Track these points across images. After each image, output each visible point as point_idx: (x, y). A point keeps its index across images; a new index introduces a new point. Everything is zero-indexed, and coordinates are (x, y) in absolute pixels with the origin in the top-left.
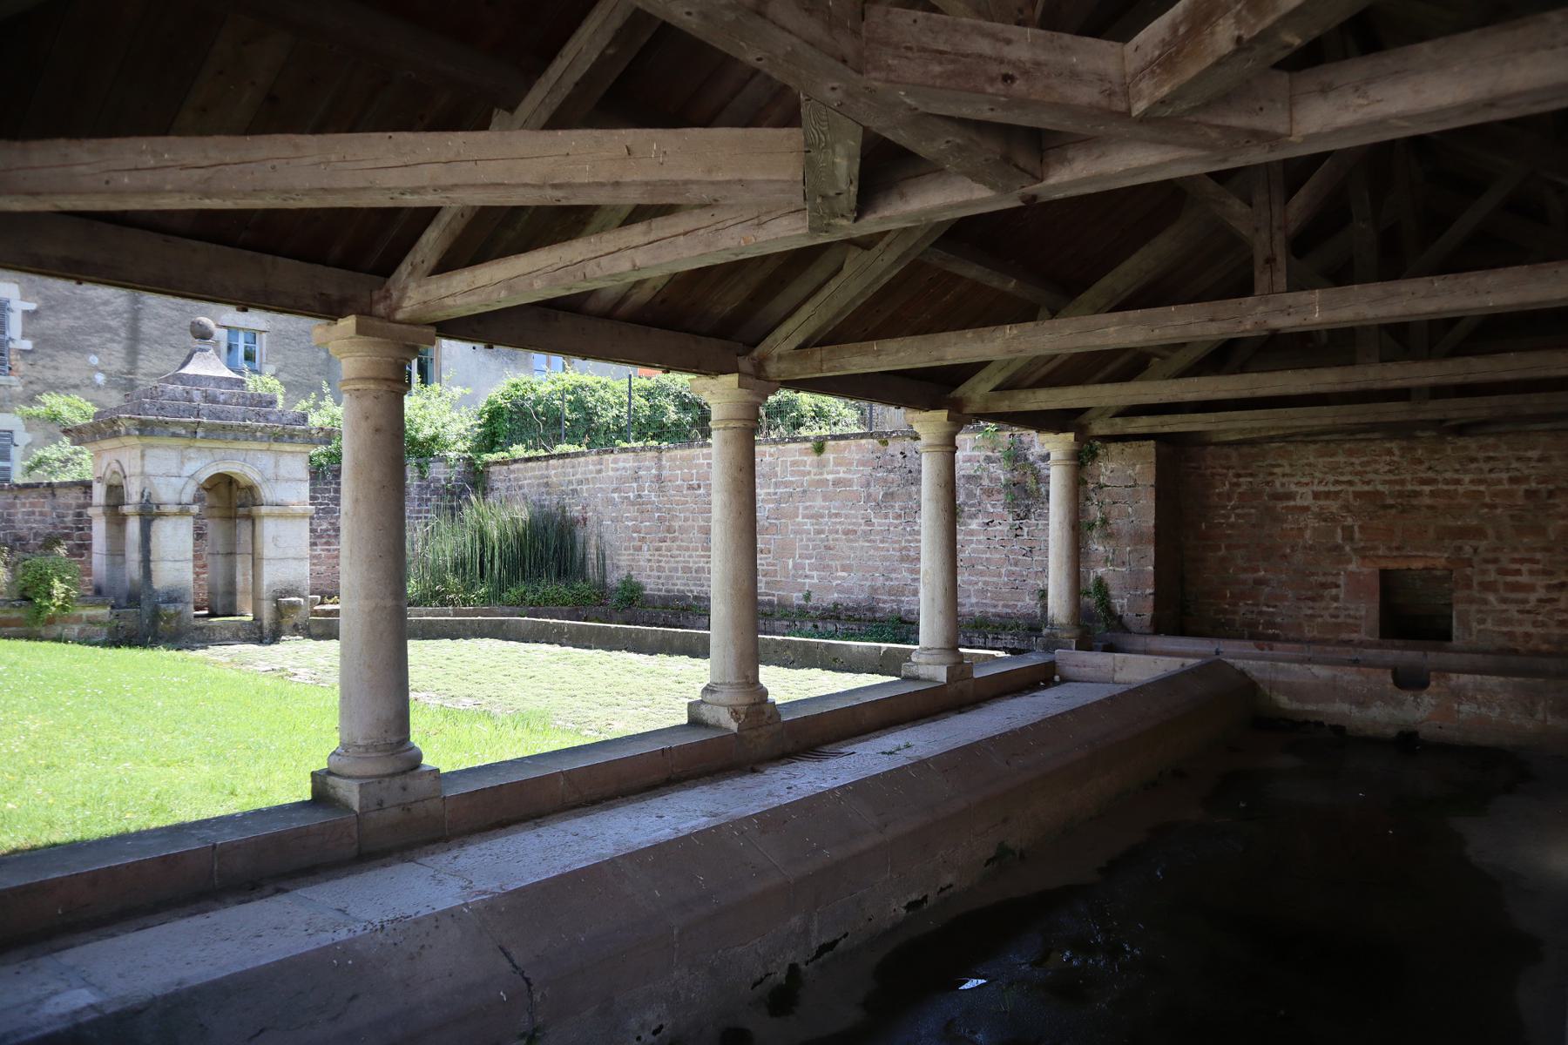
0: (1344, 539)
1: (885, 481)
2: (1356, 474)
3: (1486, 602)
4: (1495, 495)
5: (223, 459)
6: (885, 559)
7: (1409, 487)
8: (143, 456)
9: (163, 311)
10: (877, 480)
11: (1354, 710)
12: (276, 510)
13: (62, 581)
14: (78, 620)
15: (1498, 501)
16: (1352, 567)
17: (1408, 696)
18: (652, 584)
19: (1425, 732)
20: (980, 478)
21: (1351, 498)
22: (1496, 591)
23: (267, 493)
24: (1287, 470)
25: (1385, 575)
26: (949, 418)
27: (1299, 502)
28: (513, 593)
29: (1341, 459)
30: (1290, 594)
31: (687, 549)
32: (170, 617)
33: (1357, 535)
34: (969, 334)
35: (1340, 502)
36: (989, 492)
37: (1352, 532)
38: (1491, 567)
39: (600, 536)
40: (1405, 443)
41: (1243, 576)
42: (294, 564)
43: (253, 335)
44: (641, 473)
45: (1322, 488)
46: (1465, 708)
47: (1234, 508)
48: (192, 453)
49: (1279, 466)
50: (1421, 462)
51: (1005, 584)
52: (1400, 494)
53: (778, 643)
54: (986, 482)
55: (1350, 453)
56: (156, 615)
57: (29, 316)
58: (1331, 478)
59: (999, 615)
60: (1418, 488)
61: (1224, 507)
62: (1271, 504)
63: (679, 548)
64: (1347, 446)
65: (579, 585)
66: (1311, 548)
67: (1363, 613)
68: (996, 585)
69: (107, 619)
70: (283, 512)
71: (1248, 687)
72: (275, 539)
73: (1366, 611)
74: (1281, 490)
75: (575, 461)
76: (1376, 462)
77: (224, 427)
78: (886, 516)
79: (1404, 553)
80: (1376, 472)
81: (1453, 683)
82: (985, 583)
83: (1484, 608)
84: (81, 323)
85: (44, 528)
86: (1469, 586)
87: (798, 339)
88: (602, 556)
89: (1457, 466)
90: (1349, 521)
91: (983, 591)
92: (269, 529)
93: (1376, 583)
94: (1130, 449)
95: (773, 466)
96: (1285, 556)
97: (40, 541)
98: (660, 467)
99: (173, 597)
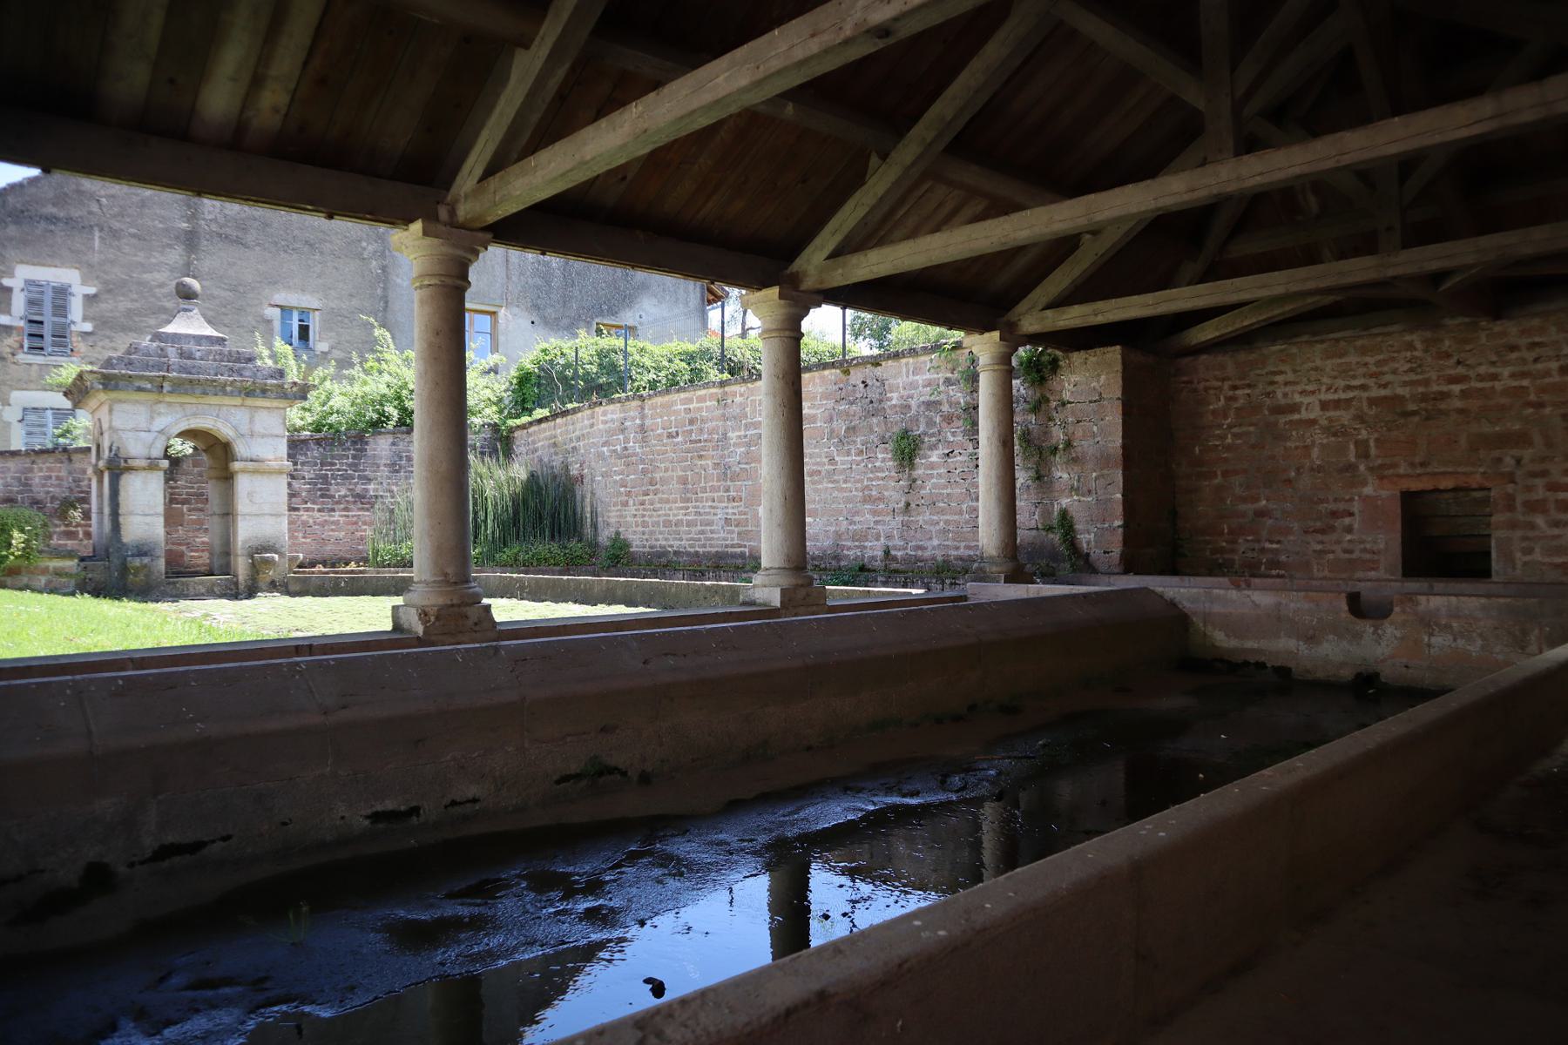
0: (1358, 456)
1: (847, 414)
2: (1371, 376)
3: (1532, 526)
4: (1543, 390)
5: (195, 415)
6: (848, 500)
7: (1435, 388)
8: (111, 411)
9: (216, 292)
10: (840, 414)
11: (1302, 646)
12: (250, 465)
13: (22, 531)
14: (45, 571)
15: (1546, 397)
16: (1368, 490)
17: (1367, 627)
18: (638, 542)
19: (1388, 673)
20: (939, 403)
21: (1365, 408)
22: (1545, 511)
23: (241, 449)
24: (1290, 377)
25: (1409, 499)
26: (781, 296)
27: (1304, 415)
28: (508, 553)
29: (1353, 359)
30: (1296, 526)
31: (667, 501)
32: (137, 570)
33: (1373, 451)
34: (603, 123)
35: (1352, 411)
36: (949, 419)
37: (1368, 446)
38: (1539, 482)
39: (593, 494)
40: (1428, 334)
41: (1242, 507)
42: (271, 520)
43: (304, 312)
44: (627, 424)
45: (1330, 396)
46: (1438, 640)
47: (1230, 427)
48: (162, 408)
49: (1281, 372)
50: (1448, 356)
51: (967, 522)
52: (1424, 398)
53: (707, 588)
54: (945, 408)
55: (1363, 351)
56: (124, 569)
57: (90, 299)
58: (1341, 383)
59: (961, 559)
60: (1445, 388)
61: (1220, 426)
62: (1272, 418)
63: (661, 501)
64: (1359, 343)
65: (573, 543)
66: (1320, 469)
67: (1382, 546)
68: (957, 524)
69: (75, 571)
70: (259, 467)
71: (1177, 620)
72: (250, 494)
73: (1387, 542)
74: (1283, 402)
75: (575, 417)
76: (1393, 359)
77: (191, 381)
78: (848, 453)
79: (1429, 470)
80: (1394, 372)
81: (1421, 608)
82: (947, 522)
83: (1530, 534)
84: (138, 305)
85: (61, 493)
86: (1510, 507)
87: (478, 172)
88: (594, 513)
89: (1494, 358)
90: (1364, 434)
91: (945, 531)
92: (244, 485)
93: (1396, 509)
94: (1094, 357)
95: (743, 406)
96: (1289, 481)
97: (56, 504)
98: (643, 417)
99: (142, 551)
